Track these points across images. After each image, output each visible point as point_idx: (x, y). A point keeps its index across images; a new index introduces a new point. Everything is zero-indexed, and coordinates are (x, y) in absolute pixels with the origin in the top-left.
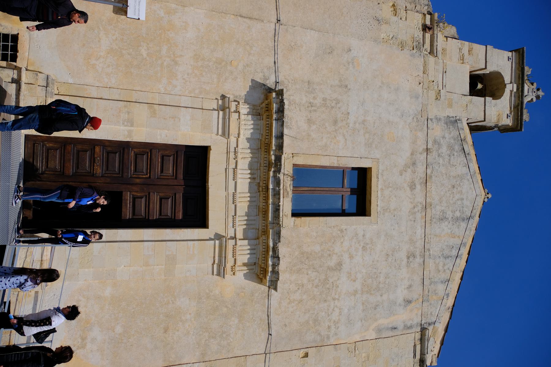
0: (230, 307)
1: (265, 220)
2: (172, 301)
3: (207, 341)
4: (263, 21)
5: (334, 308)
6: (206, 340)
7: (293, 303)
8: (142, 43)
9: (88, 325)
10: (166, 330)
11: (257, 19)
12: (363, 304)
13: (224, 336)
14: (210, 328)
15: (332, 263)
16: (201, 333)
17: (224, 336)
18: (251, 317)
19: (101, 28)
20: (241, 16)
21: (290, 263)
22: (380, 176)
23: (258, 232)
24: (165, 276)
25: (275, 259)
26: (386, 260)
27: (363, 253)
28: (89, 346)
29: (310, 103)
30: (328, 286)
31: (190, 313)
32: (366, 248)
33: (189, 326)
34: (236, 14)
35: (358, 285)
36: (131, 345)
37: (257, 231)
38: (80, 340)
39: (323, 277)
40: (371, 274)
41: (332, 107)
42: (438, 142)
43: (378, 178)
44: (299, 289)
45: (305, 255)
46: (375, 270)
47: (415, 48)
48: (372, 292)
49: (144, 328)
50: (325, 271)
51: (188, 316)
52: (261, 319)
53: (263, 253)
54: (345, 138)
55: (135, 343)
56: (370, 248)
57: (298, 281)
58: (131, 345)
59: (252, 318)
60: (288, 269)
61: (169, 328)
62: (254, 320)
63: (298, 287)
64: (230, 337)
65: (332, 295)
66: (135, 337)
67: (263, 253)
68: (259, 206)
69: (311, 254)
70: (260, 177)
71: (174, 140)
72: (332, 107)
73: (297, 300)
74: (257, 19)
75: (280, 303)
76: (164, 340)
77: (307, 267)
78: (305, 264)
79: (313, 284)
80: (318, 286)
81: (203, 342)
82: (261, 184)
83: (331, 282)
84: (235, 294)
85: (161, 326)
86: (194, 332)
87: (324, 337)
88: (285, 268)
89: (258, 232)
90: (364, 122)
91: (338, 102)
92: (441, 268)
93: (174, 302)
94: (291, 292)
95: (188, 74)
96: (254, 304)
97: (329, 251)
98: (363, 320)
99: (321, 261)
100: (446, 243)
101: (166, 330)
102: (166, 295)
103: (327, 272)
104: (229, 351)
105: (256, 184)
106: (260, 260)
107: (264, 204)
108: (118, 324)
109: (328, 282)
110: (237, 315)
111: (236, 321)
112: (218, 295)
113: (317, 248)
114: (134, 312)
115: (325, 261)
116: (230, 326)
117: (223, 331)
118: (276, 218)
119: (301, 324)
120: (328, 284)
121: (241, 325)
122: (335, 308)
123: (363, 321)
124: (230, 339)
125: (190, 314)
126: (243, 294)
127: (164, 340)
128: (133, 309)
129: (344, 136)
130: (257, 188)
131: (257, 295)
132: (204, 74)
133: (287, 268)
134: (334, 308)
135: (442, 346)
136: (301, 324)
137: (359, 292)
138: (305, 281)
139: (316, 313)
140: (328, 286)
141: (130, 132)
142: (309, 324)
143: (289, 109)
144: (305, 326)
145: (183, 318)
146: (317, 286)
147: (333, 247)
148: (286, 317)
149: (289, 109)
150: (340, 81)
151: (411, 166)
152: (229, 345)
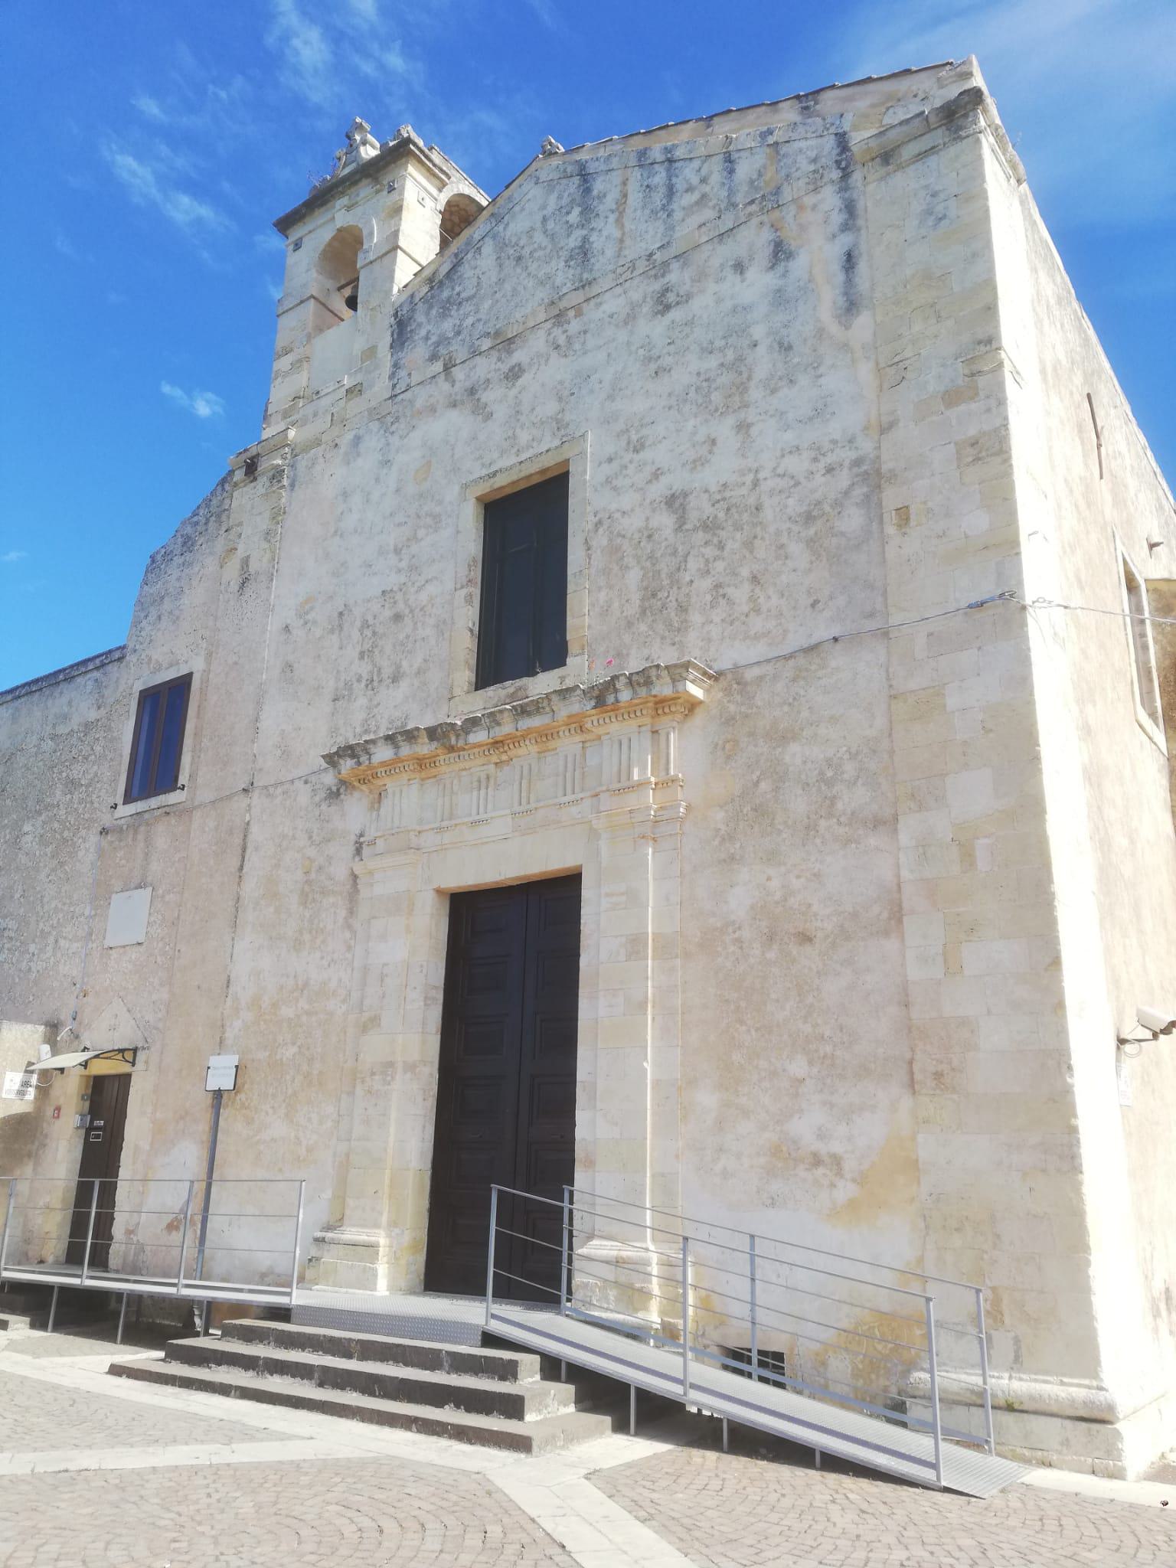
0: (758, 773)
1: (558, 732)
2: (734, 932)
3: (842, 819)
4: (248, 823)
5: (779, 475)
6: (839, 823)
7: (760, 600)
8: (278, 1057)
9: (784, 1149)
10: (805, 938)
11: (245, 836)
12: (773, 391)
13: (830, 774)
14: (809, 818)
15: (665, 521)
16: (818, 841)
17: (830, 774)
18: (786, 708)
19: (258, 1137)
20: (241, 868)
21: (663, 638)
22: (494, 468)
23: (589, 741)
24: (677, 957)
25: (617, 686)
26: (670, 371)
27: (650, 445)
28: (837, 1147)
29: (367, 686)
30: (721, 515)
31: (767, 880)
32: (637, 441)
33: (798, 877)
34: (237, 880)
35: (724, 429)
36: (841, 1030)
37: (588, 744)
38: (820, 1171)
39: (700, 536)
40: (700, 401)
41: (374, 633)
42: (435, 348)
43: (495, 474)
44: (724, 596)
45: (647, 604)
46: (692, 393)
47: (280, 485)
48: (745, 375)
49: (798, 999)
50: (684, 537)
51: (775, 884)
52: (794, 680)
53: (620, 718)
54: (424, 585)
55: (837, 1020)
56: (637, 432)
57: (705, 604)
58: (841, 1030)
59: (790, 704)
60: (677, 639)
61: (801, 930)
62: (794, 699)
63: (720, 599)
64: (835, 755)
65: (743, 495)
66: (820, 1021)
67: (620, 718)
68: (539, 752)
69: (646, 589)
70: (483, 765)
71: (421, 971)
72: (374, 633)
73: (753, 591)
74: (245, 836)
75: (757, 637)
76: (830, 940)
77: (675, 588)
78: (668, 596)
79: (715, 560)
80: (720, 542)
81: (842, 830)
82: (495, 759)
83: (711, 509)
84: (728, 768)
85: (795, 952)
86: (817, 860)
87: (857, 476)
88: (675, 647)
89: (589, 741)
90: (397, 551)
91: (366, 624)
92: (695, 197)
93: (737, 926)
94: (730, 616)
95: (322, 958)
96: (755, 710)
97: (640, 542)
98: (819, 373)
99: (661, 556)
100: (639, 213)
101: (805, 938)
102: (719, 949)
103: (687, 530)
104: (874, 752)
105: (499, 770)
106: (640, 721)
107: (527, 742)
108: (784, 1070)
109: (710, 519)
110: (780, 750)
111: (794, 748)
112: (726, 811)
113: (634, 577)
114: (757, 1030)
115: (663, 544)
116: (805, 762)
117: (817, 781)
118: (539, 708)
119: (814, 558)
120: (716, 517)
121: (804, 733)
122: (780, 471)
123: (822, 370)
124: (839, 755)
125: (769, 879)
126: (728, 746)
127: (830, 940)
128: (749, 1031)
129: (420, 589)
130: (508, 765)
131: (732, 708)
132: (321, 925)
133: (674, 644)
134: (779, 475)
135: (914, 68)
136: (814, 558)
137: (743, 415)
138: (706, 583)
139: (788, 525)
140: (721, 515)
141: (410, 1068)
142: (816, 533)
143: (375, 732)
144: (821, 546)
145: (778, 896)
146: (721, 547)
147: (632, 535)
148: (794, 608)
149: (375, 732)
150: (332, 631)
151: (477, 397)
152: (857, 753)
